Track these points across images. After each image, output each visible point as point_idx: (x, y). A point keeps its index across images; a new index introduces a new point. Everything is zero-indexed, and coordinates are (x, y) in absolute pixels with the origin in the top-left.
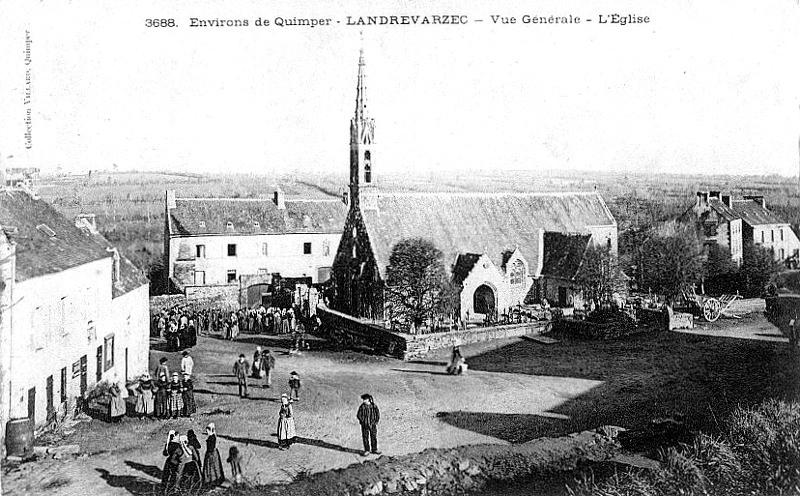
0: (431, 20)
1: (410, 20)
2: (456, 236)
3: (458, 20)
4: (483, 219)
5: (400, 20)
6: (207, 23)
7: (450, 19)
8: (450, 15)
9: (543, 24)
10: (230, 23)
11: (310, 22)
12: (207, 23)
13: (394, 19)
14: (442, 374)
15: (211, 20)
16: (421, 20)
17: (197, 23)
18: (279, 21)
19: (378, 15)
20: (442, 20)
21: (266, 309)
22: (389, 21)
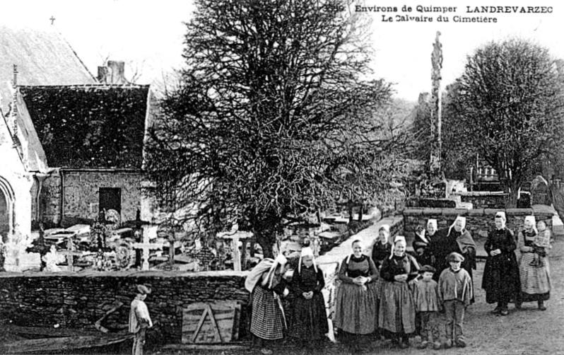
0: (527, 10)
1: (512, 9)
2: (533, 326)
3: (546, 10)
4: (153, 219)
5: (504, 10)
6: (368, 9)
7: (540, 9)
8: (540, 6)
9: (468, 23)
10: (493, 10)
11: (442, 10)
12: (368, 9)
13: (530, 9)
14: (10, 133)
15: (370, 6)
16: (519, 9)
17: (360, 8)
18: (419, 8)
19: (489, 6)
20: (534, 10)
21: (251, 47)
22: (497, 10)
